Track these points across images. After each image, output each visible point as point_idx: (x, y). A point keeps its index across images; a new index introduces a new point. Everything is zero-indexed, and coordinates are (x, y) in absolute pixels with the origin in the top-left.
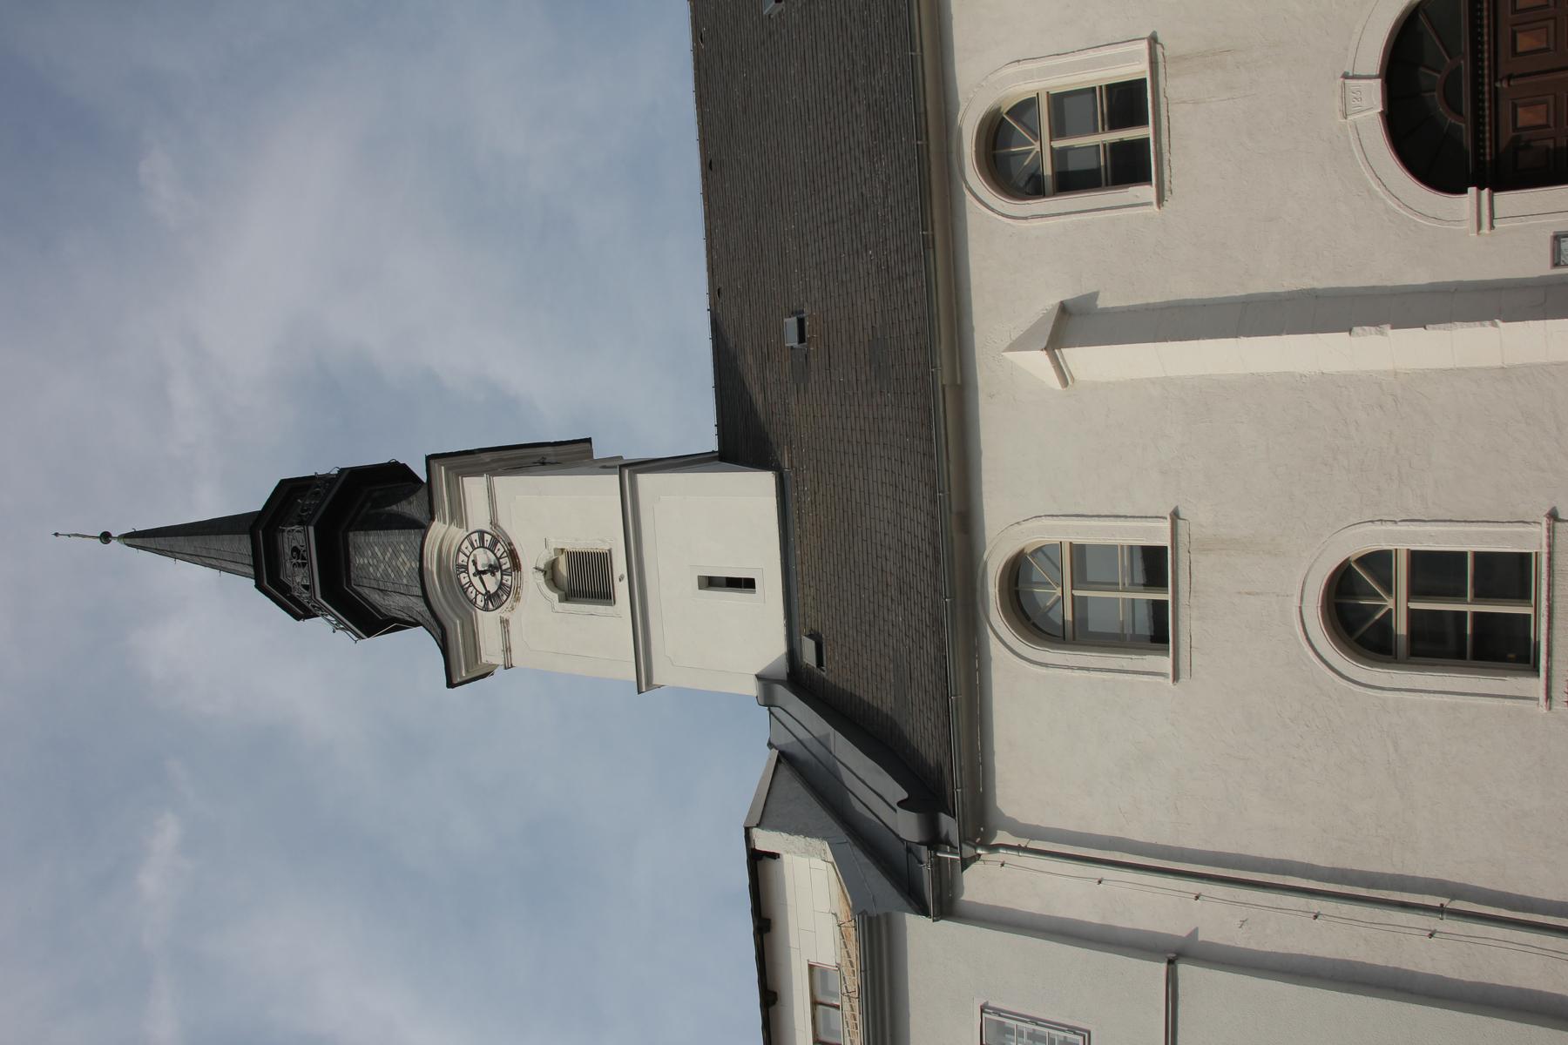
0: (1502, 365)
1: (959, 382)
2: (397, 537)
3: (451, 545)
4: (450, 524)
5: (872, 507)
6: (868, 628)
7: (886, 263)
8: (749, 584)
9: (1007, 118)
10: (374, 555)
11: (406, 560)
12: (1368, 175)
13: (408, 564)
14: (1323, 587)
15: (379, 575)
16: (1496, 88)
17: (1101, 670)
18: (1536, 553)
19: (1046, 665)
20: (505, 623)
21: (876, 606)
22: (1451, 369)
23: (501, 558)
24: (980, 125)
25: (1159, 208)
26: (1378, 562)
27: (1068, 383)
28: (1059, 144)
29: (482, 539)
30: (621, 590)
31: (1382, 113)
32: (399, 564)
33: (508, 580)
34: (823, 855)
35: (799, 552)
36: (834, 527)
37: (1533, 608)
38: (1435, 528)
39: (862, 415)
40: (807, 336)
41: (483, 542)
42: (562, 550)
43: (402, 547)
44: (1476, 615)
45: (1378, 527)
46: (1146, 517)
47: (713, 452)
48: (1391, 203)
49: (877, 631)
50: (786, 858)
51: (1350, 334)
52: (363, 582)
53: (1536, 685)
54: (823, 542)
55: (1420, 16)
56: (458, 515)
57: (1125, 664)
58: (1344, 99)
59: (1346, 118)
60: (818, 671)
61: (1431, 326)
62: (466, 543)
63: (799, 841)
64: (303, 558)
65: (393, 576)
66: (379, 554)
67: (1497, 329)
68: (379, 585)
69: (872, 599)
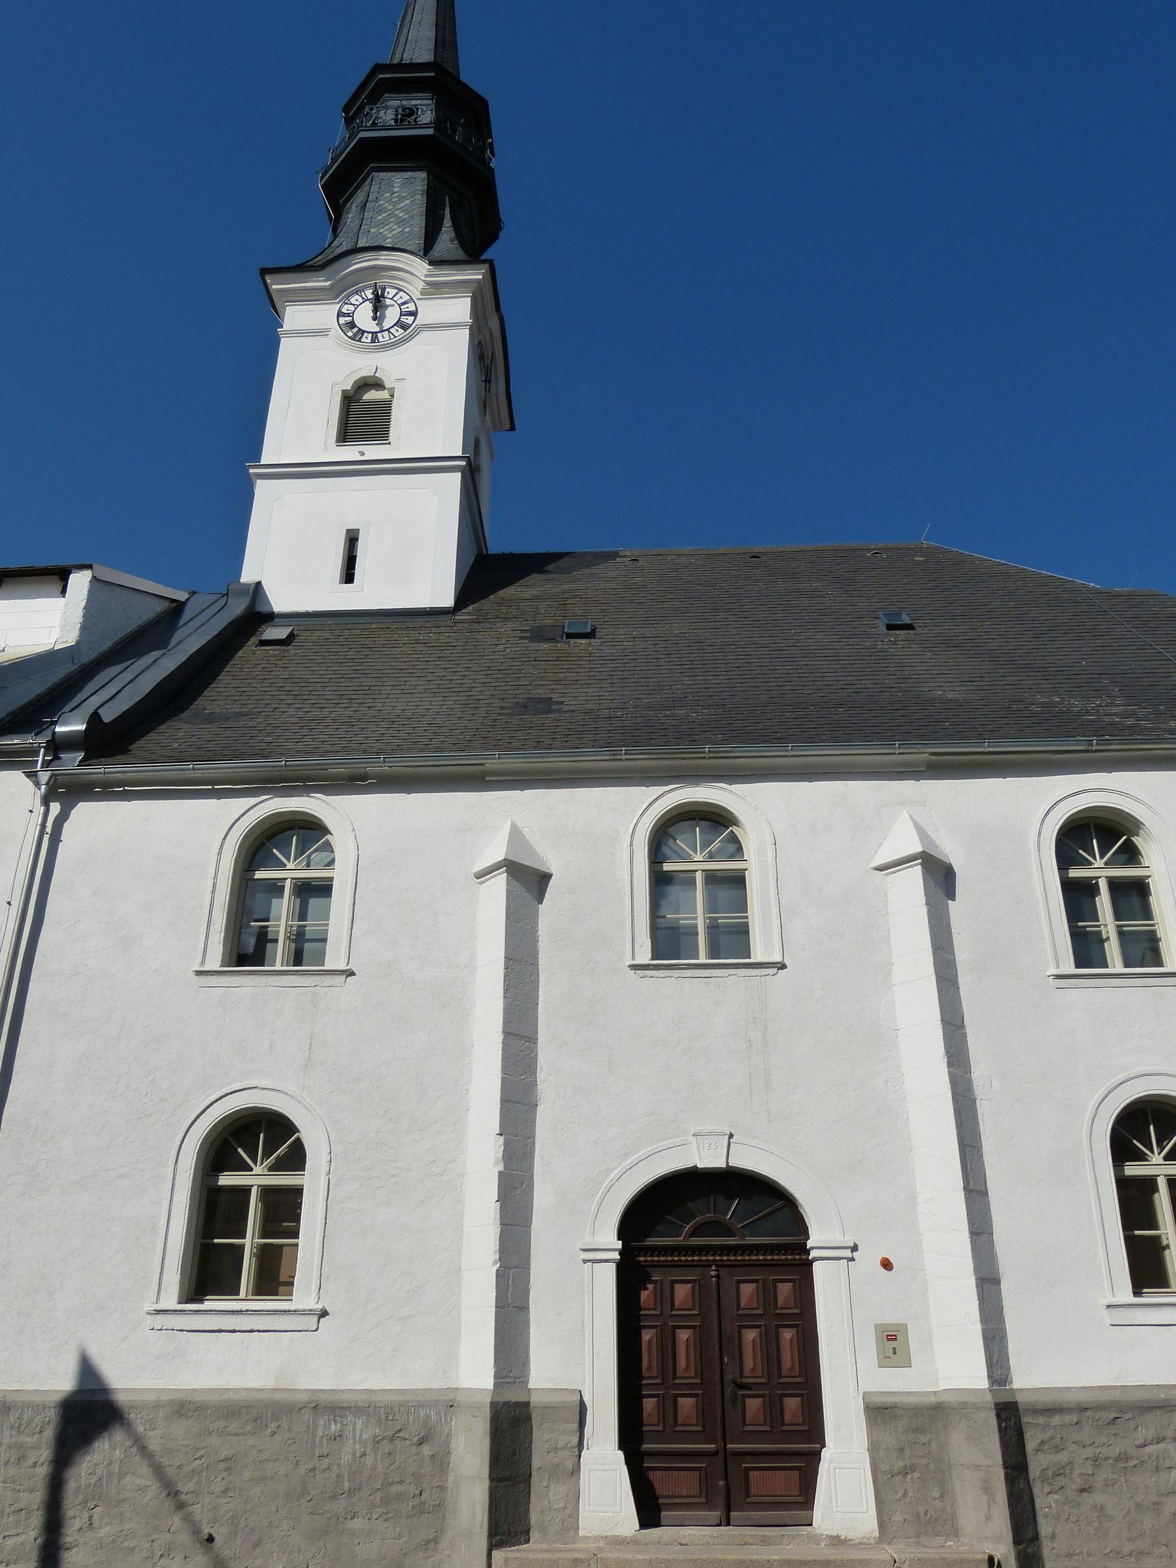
0: (463, 1269)
1: (487, 779)
2: (418, 223)
3: (401, 280)
4: (428, 283)
5: (399, 696)
6: (287, 689)
7: (615, 716)
8: (348, 576)
9: (728, 830)
10: (402, 199)
11: (395, 232)
12: (642, 1153)
13: (390, 234)
14: (274, 1108)
15: (382, 202)
16: (711, 1266)
17: (212, 905)
18: (292, 1300)
19: (220, 853)
20: (321, 333)
21: (305, 697)
22: (462, 1225)
23: (389, 332)
24: (721, 806)
25: (629, 966)
26: (296, 1159)
27: (477, 879)
28: (699, 878)
29: (411, 314)
30: (350, 452)
31: (695, 1167)
32: (391, 225)
33: (367, 338)
34: (61, 640)
35: (374, 627)
36: (388, 660)
37: (244, 1298)
38: (320, 1209)
39: (485, 689)
40: (572, 641)
41: (405, 315)
42: (392, 396)
43: (407, 230)
44: (242, 1247)
45: (325, 1158)
46: (350, 947)
47: (487, 549)
48: (614, 1174)
49: (283, 697)
50: (60, 602)
51: (498, 1134)
52: (375, 185)
53: (170, 1300)
54: (379, 649)
55: (782, 1202)
56: (434, 290)
57: (216, 926)
58: (711, 1134)
59: (693, 1136)
60: (254, 640)
61: (499, 1207)
62: (406, 298)
63: (77, 617)
64: (402, 120)
65: (379, 218)
66: (403, 204)
67: (491, 1265)
68: (371, 202)
69: (314, 693)
